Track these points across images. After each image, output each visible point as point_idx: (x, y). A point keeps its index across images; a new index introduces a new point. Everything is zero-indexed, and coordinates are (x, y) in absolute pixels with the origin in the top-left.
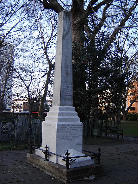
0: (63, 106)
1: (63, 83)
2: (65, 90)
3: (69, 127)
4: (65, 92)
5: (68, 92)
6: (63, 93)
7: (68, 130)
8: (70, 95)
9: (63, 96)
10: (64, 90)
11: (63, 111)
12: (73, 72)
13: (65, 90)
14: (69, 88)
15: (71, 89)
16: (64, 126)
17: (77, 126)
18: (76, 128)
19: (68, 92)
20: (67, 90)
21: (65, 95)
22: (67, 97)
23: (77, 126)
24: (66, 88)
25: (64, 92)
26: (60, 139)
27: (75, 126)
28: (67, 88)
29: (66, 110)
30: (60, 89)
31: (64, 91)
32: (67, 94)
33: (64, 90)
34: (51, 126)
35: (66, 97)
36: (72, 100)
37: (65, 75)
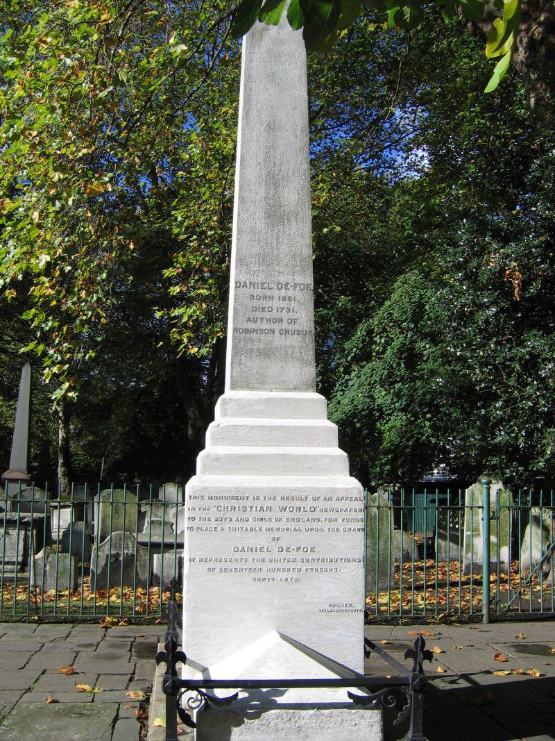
0: (253, 389)
1: (254, 268)
2: (267, 304)
3: (269, 503)
4: (266, 315)
5: (284, 315)
6: (249, 319)
7: (265, 525)
8: (297, 327)
9: (254, 336)
10: (255, 303)
11: (245, 414)
12: (313, 220)
13: (267, 304)
14: (291, 292)
15: (308, 298)
16: (233, 498)
17: (322, 504)
18: (315, 515)
19: (284, 315)
20: (276, 303)
21: (262, 331)
22: (278, 340)
23: (322, 504)
24: (267, 292)
25: (258, 314)
26: (212, 570)
27: (310, 503)
28: (276, 293)
29: (254, 414)
30: (363, 583)
31: (255, 309)
32: (276, 327)
33: (255, 303)
34: (38, 679)
35: (270, 343)
36: (310, 355)
37: (261, 225)
